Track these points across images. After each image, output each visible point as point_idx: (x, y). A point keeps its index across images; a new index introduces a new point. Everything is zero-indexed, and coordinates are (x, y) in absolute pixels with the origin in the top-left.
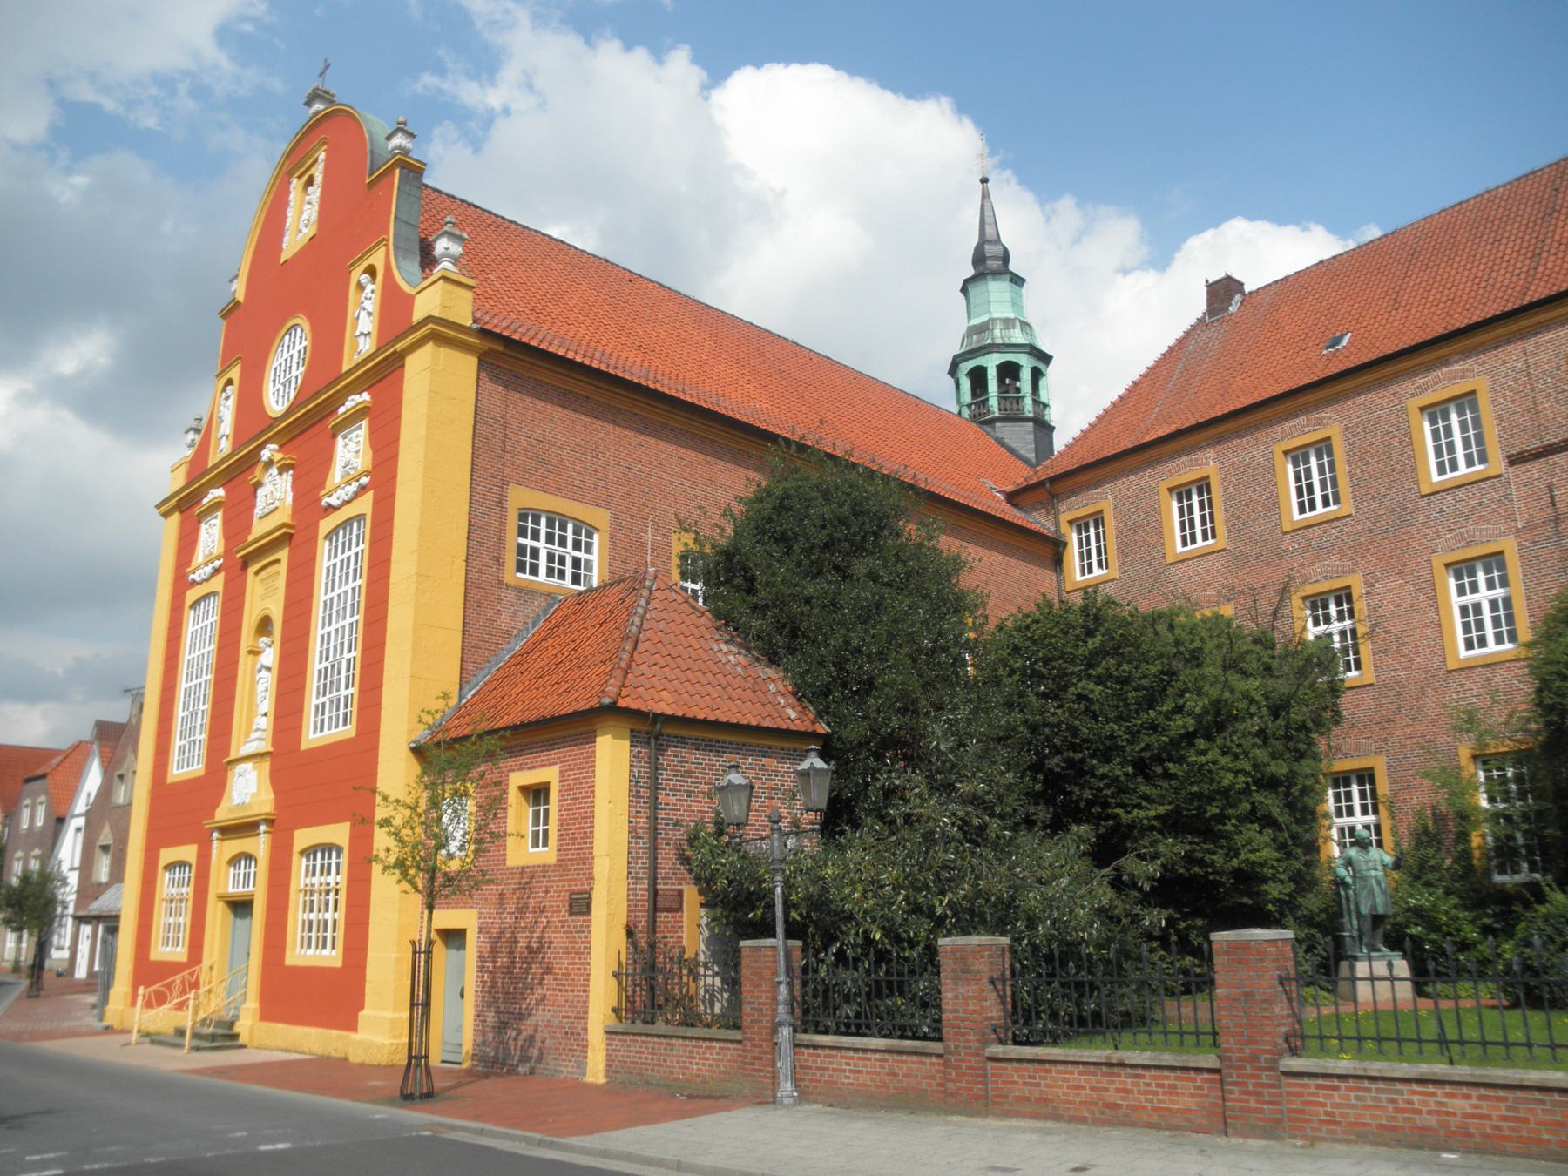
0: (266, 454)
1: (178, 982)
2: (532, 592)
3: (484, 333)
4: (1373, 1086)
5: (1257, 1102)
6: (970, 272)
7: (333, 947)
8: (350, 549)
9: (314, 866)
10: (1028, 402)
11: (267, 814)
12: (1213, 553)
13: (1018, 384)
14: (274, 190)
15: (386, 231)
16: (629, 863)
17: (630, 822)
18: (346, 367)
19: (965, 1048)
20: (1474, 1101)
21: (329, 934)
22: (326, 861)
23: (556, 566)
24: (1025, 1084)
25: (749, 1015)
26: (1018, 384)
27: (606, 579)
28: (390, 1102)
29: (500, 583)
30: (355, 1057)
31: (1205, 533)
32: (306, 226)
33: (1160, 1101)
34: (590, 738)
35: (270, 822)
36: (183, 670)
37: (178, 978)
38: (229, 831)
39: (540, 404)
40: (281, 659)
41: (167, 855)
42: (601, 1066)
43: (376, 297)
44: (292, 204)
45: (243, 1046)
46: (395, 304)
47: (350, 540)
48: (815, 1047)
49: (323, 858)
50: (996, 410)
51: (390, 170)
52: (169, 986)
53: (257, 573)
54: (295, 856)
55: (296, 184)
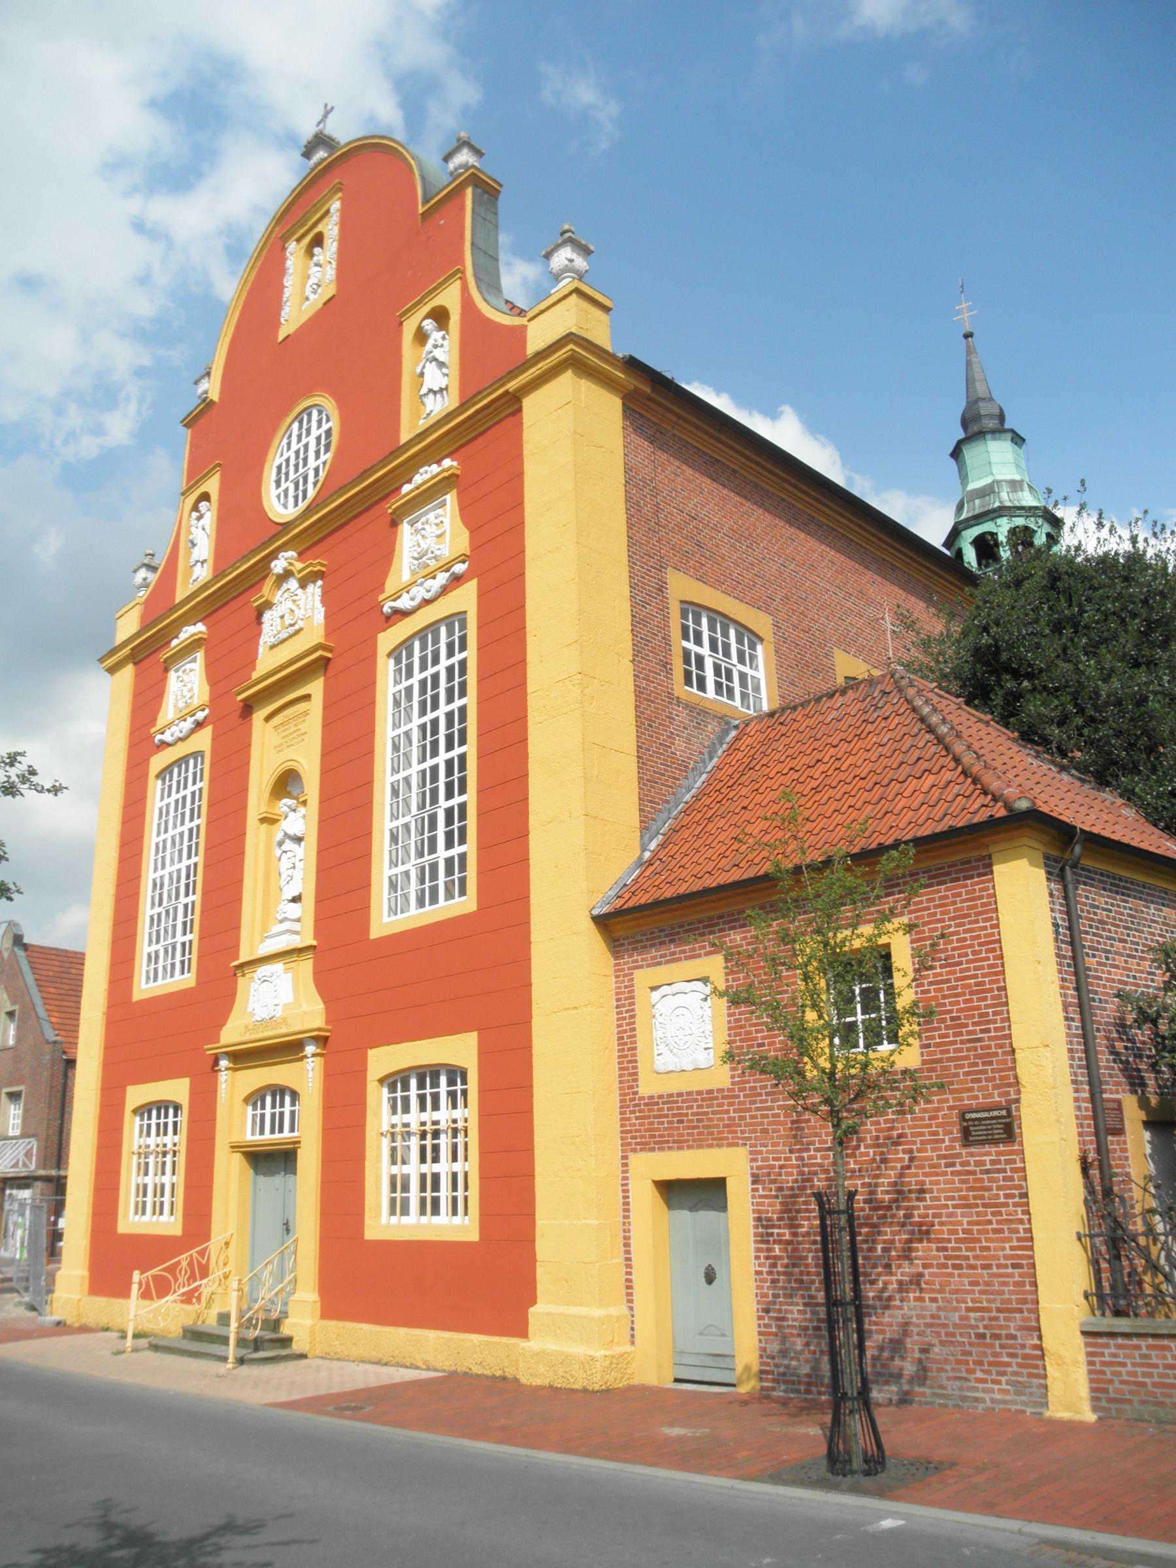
0: (278, 566)
1: (184, 1264)
2: (704, 712)
3: (632, 364)
4: (1112, 1342)
7: (466, 1214)
8: (185, 787)
9: (149, 1126)
11: (319, 1029)
14: (259, 264)
15: (461, 261)
18: (178, 599)
21: (167, 1199)
22: (162, 1120)
23: (724, 680)
27: (776, 705)
28: (799, 1477)
30: (532, 1375)
32: (315, 292)
34: (985, 866)
35: (322, 1040)
36: (149, 856)
37: (184, 1259)
38: (244, 1057)
39: (689, 471)
41: (137, 1095)
44: (291, 271)
45: (303, 1356)
47: (186, 779)
49: (159, 1117)
51: (458, 191)
52: (172, 1269)
53: (268, 719)
54: (372, 1086)
55: (293, 250)
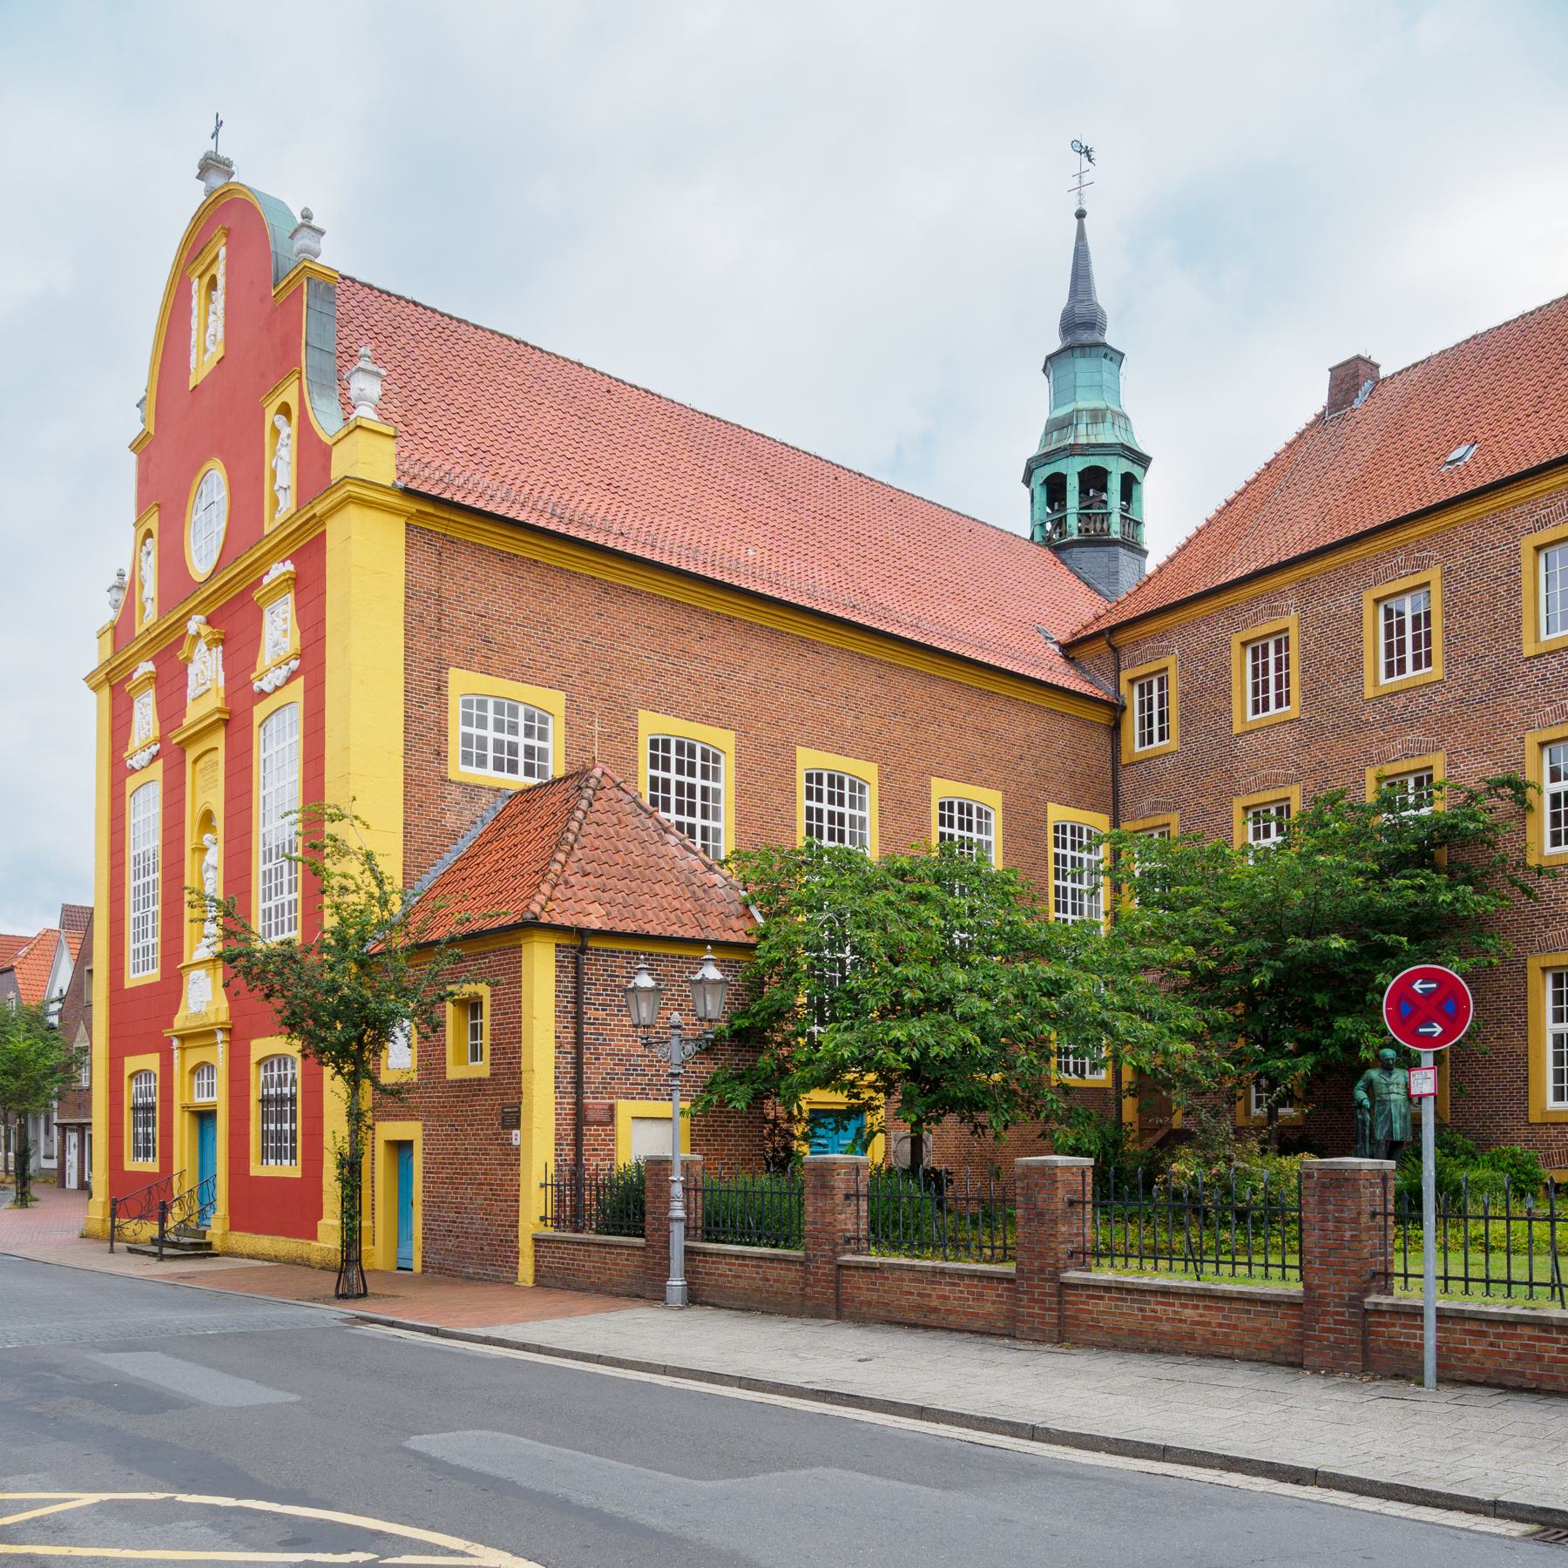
3: (407, 492)
5: (1040, 1309)
6: (1056, 344)
10: (1115, 521)
11: (222, 1023)
12: (1285, 722)
13: (1104, 497)
16: (556, 1077)
17: (557, 1037)
19: (822, 1256)
20: (1201, 1311)
24: (868, 1289)
25: (651, 1224)
26: (1104, 497)
29: (444, 779)
31: (1417, 659)
33: (969, 1307)
40: (226, 858)
41: (132, 1064)
42: (531, 1271)
43: (293, 442)
46: (314, 454)
48: (705, 1254)
50: (1076, 532)
54: (253, 1067)
55: (197, 287)
